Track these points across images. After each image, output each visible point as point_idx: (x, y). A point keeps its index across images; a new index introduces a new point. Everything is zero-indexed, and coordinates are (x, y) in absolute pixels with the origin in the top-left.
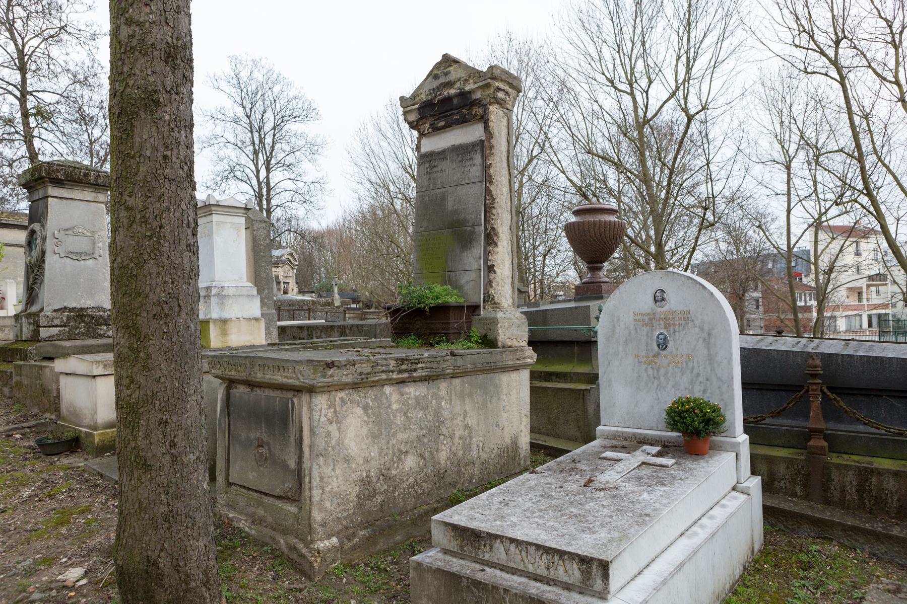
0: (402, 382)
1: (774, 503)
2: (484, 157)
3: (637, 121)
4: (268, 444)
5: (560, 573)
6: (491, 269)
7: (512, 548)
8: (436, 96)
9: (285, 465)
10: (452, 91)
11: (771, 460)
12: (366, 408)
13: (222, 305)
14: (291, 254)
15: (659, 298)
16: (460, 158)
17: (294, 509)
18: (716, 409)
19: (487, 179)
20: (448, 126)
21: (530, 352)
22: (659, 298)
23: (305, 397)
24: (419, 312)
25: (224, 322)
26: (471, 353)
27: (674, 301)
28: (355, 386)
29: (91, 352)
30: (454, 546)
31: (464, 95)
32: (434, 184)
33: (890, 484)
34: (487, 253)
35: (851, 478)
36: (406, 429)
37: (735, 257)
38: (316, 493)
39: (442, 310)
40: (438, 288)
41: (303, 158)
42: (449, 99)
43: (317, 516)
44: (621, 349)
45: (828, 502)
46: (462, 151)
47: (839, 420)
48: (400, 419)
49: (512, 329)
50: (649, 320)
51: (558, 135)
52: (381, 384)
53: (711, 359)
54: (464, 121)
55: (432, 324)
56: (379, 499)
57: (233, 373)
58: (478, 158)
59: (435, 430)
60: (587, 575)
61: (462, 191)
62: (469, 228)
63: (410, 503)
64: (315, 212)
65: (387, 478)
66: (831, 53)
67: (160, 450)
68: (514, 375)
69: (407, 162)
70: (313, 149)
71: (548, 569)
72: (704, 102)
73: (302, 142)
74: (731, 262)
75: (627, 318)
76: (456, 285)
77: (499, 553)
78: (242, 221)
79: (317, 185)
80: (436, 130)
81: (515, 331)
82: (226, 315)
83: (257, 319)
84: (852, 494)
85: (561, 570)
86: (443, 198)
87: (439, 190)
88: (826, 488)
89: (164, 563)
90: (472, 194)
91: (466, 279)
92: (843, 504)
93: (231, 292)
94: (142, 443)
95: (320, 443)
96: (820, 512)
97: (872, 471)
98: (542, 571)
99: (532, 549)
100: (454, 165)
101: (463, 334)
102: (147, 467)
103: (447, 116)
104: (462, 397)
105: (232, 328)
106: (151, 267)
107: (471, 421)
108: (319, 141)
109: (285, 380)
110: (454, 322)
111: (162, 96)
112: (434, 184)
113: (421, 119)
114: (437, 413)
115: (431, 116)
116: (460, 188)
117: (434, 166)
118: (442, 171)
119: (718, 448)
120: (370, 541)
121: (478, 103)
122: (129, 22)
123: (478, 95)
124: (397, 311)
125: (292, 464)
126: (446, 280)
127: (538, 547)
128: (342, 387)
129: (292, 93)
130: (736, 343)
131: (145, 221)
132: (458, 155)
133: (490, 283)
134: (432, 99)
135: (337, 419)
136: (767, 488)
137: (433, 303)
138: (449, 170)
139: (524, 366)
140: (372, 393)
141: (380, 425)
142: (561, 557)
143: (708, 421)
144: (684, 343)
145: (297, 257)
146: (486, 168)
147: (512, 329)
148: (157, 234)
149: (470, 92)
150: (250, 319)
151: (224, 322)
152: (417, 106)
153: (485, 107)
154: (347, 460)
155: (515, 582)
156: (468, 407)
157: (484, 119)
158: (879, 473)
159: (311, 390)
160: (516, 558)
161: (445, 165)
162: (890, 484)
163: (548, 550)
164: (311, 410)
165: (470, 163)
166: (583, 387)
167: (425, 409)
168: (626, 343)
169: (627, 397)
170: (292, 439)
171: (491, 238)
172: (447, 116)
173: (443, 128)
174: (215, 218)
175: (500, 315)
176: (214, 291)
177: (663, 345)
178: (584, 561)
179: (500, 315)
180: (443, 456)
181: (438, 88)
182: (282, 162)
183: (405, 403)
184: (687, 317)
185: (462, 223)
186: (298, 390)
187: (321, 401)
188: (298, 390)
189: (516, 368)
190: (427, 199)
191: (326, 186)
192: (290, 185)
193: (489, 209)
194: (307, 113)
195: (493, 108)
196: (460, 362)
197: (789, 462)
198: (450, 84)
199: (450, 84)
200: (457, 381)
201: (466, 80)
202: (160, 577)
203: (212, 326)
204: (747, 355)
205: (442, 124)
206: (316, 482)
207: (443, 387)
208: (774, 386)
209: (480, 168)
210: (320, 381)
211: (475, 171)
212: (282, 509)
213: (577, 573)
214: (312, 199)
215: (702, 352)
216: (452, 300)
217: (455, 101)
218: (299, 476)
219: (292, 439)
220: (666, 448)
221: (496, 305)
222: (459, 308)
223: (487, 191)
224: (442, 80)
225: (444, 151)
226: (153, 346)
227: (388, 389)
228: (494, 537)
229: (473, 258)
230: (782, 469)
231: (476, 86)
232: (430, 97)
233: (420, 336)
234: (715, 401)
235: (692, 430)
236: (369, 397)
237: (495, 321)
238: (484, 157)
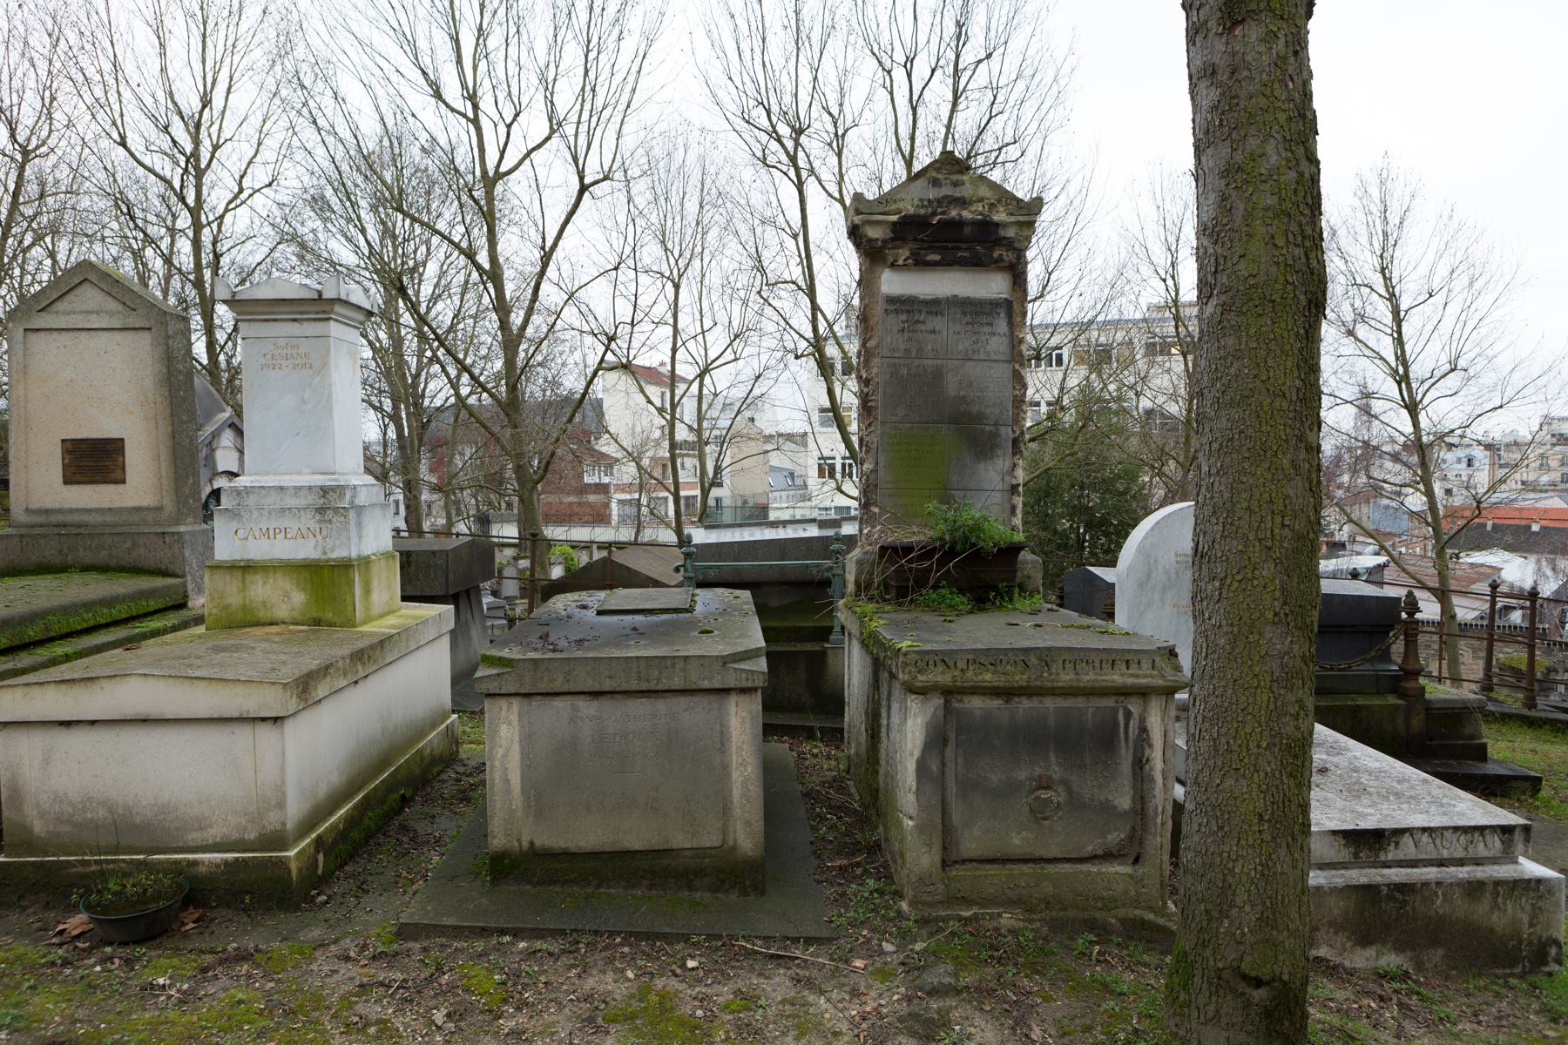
3: (484, 172)
4: (1065, 783)
5: (1481, 850)
7: (1425, 838)
8: (934, 214)
9: (1107, 809)
10: (966, 214)
16: (968, 319)
20: (947, 263)
29: (500, 658)
30: (1345, 855)
32: (920, 350)
42: (959, 224)
44: (1156, 597)
46: (975, 310)
54: (976, 263)
57: (988, 677)
58: (1002, 325)
61: (972, 370)
62: (988, 428)
71: (1466, 849)
72: (606, 169)
77: (1408, 849)
85: (1481, 846)
86: (938, 375)
87: (930, 362)
98: (1459, 854)
99: (1448, 834)
100: (958, 328)
103: (946, 248)
109: (1130, 681)
112: (920, 350)
113: (892, 239)
115: (915, 239)
116: (969, 364)
117: (918, 322)
118: (933, 332)
123: (1010, 233)
125: (1124, 802)
127: (1456, 829)
132: (964, 314)
134: (926, 217)
142: (1482, 835)
149: (997, 225)
152: (894, 218)
155: (1431, 873)
161: (938, 323)
165: (987, 329)
166: (809, 647)
168: (1164, 589)
172: (946, 248)
173: (934, 264)
174: (335, 329)
181: (939, 201)
185: (980, 418)
190: (904, 371)
199: (963, 202)
201: (992, 205)
205: (937, 257)
209: (1005, 340)
212: (1100, 873)
213: (1498, 844)
217: (967, 230)
219: (1126, 766)
224: (947, 191)
225: (936, 302)
228: (1399, 832)
231: (1013, 219)
232: (922, 212)
238: (1011, 325)
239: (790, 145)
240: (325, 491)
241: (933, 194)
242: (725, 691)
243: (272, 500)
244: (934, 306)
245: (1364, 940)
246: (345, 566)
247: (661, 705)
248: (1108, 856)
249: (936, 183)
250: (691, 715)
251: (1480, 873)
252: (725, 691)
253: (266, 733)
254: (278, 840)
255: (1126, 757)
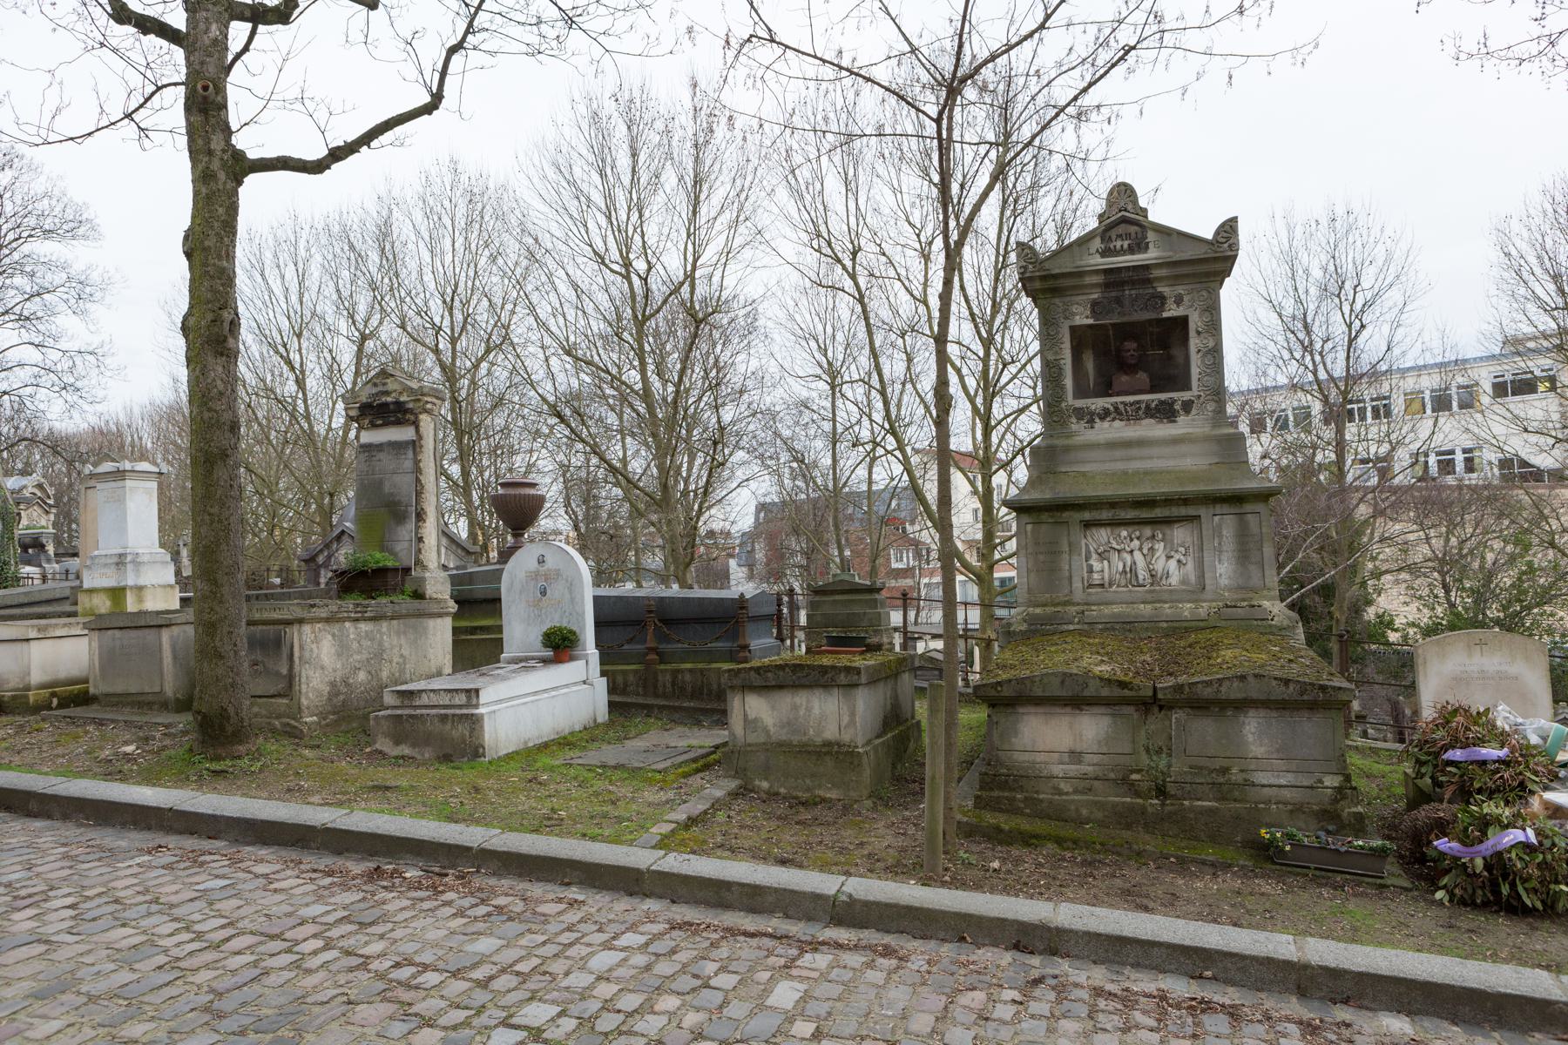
0: (357, 620)
1: (617, 699)
2: (415, 454)
6: (420, 540)
9: (278, 674)
10: (389, 399)
11: (614, 672)
12: (333, 635)
13: (137, 572)
14: (40, 486)
15: (541, 561)
17: (285, 701)
18: (573, 633)
19: (417, 470)
20: (386, 424)
21: (452, 603)
22: (541, 561)
23: (296, 627)
24: (363, 574)
25: (140, 588)
26: (405, 604)
27: (551, 563)
28: (327, 620)
31: (398, 403)
33: (688, 677)
34: (418, 528)
35: (668, 677)
36: (359, 652)
37: (803, 496)
38: (304, 687)
39: (382, 572)
40: (378, 555)
41: (62, 307)
42: (386, 404)
43: (304, 702)
45: (656, 696)
46: (397, 447)
47: (668, 642)
48: (355, 645)
49: (438, 586)
50: (535, 576)
51: (522, 328)
52: (343, 620)
53: (572, 600)
55: (374, 583)
56: (342, 697)
58: (410, 454)
59: (379, 655)
60: (469, 698)
61: (397, 479)
63: (362, 704)
64: (86, 407)
65: (347, 685)
66: (849, 264)
67: (228, 648)
68: (439, 621)
69: (279, 340)
70: (82, 292)
73: (60, 278)
74: (798, 506)
75: (521, 575)
76: (395, 554)
78: (155, 485)
79: (91, 358)
80: (374, 426)
81: (440, 587)
82: (141, 582)
83: (171, 586)
84: (669, 688)
86: (381, 482)
88: (655, 687)
89: (231, 710)
90: (404, 483)
91: (400, 547)
92: (665, 696)
93: (145, 559)
94: (218, 644)
95: (307, 654)
96: (650, 701)
97: (678, 671)
98: (447, 702)
101: (398, 589)
102: (221, 657)
104: (398, 633)
105: (148, 595)
106: (224, 547)
107: (406, 652)
108: (95, 277)
110: (391, 580)
111: (229, 452)
114: (380, 644)
119: (572, 659)
120: (336, 723)
121: (411, 411)
122: (209, 410)
123: (411, 405)
124: (343, 573)
125: (284, 671)
126: (382, 549)
128: (320, 620)
129: (38, 187)
130: (588, 592)
131: (220, 521)
133: (419, 551)
135: (316, 641)
136: (612, 690)
137: (375, 566)
138: (385, 460)
139: (447, 614)
140: (337, 626)
141: (343, 649)
143: (564, 639)
144: (557, 591)
145: (51, 491)
146: (417, 462)
147: (438, 586)
148: (227, 529)
150: (164, 586)
151: (140, 589)
153: (416, 415)
154: (323, 668)
155: (424, 711)
156: (403, 641)
157: (416, 424)
158: (682, 671)
159: (301, 621)
160: (434, 699)
161: (381, 456)
162: (688, 677)
163: (450, 691)
164: (300, 634)
167: (372, 640)
169: (520, 629)
170: (285, 656)
171: (420, 516)
174: (128, 483)
175: (427, 575)
176: (129, 558)
177: (544, 593)
178: (468, 691)
179: (427, 575)
180: (385, 674)
182: (17, 310)
183: (359, 635)
184: (558, 573)
185: (399, 503)
186: (289, 623)
187: (307, 628)
188: (289, 623)
189: (440, 615)
191: (108, 361)
192: (32, 355)
193: (419, 494)
194: (73, 227)
195: (423, 417)
196: (397, 608)
197: (636, 671)
198: (387, 393)
199: (387, 393)
200: (395, 622)
202: (229, 718)
203: (128, 593)
204: (596, 599)
206: (303, 680)
207: (385, 625)
208: (616, 622)
210: (306, 615)
211: (408, 464)
214: (79, 384)
215: (567, 596)
216: (390, 564)
218: (291, 678)
219: (285, 656)
220: (546, 661)
221: (425, 568)
222: (396, 570)
223: (418, 480)
224: (380, 388)
226: (225, 590)
227: (347, 624)
229: (406, 531)
230: (631, 678)
233: (362, 592)
234: (574, 628)
235: (560, 645)
236: (336, 628)
237: (423, 579)
238: (415, 454)
239: (849, 264)
240: (120, 555)
241: (374, 391)
242: (160, 626)
243: (103, 560)
244: (380, 447)
245: (397, 743)
246: (123, 589)
247: (139, 633)
248: (279, 695)
249: (375, 385)
250: (150, 635)
251: (458, 712)
252: (160, 626)
253: (25, 645)
254: (28, 688)
255: (285, 651)
